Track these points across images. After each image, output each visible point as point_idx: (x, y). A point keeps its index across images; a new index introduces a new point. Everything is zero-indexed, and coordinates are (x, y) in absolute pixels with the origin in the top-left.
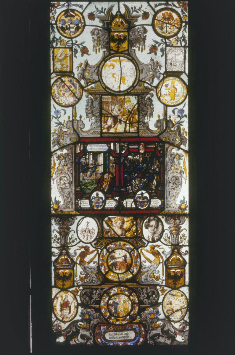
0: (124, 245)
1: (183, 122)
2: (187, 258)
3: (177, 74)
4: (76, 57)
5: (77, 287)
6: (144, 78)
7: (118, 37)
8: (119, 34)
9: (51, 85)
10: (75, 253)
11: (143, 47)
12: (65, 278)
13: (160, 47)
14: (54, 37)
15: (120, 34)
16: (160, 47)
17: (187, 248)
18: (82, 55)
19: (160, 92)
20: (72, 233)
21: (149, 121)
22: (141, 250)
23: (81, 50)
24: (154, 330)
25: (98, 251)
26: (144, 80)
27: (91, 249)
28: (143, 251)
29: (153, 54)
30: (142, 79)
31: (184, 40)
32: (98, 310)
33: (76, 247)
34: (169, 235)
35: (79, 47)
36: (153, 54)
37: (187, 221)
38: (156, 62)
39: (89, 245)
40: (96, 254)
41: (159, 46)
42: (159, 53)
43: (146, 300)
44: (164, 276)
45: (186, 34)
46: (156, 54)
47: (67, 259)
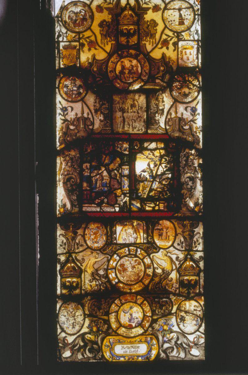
8: (129, 27)
18: (89, 50)
23: (88, 45)
36: (165, 48)
41: (171, 40)
42: (171, 47)
44: (177, 284)
46: (168, 48)
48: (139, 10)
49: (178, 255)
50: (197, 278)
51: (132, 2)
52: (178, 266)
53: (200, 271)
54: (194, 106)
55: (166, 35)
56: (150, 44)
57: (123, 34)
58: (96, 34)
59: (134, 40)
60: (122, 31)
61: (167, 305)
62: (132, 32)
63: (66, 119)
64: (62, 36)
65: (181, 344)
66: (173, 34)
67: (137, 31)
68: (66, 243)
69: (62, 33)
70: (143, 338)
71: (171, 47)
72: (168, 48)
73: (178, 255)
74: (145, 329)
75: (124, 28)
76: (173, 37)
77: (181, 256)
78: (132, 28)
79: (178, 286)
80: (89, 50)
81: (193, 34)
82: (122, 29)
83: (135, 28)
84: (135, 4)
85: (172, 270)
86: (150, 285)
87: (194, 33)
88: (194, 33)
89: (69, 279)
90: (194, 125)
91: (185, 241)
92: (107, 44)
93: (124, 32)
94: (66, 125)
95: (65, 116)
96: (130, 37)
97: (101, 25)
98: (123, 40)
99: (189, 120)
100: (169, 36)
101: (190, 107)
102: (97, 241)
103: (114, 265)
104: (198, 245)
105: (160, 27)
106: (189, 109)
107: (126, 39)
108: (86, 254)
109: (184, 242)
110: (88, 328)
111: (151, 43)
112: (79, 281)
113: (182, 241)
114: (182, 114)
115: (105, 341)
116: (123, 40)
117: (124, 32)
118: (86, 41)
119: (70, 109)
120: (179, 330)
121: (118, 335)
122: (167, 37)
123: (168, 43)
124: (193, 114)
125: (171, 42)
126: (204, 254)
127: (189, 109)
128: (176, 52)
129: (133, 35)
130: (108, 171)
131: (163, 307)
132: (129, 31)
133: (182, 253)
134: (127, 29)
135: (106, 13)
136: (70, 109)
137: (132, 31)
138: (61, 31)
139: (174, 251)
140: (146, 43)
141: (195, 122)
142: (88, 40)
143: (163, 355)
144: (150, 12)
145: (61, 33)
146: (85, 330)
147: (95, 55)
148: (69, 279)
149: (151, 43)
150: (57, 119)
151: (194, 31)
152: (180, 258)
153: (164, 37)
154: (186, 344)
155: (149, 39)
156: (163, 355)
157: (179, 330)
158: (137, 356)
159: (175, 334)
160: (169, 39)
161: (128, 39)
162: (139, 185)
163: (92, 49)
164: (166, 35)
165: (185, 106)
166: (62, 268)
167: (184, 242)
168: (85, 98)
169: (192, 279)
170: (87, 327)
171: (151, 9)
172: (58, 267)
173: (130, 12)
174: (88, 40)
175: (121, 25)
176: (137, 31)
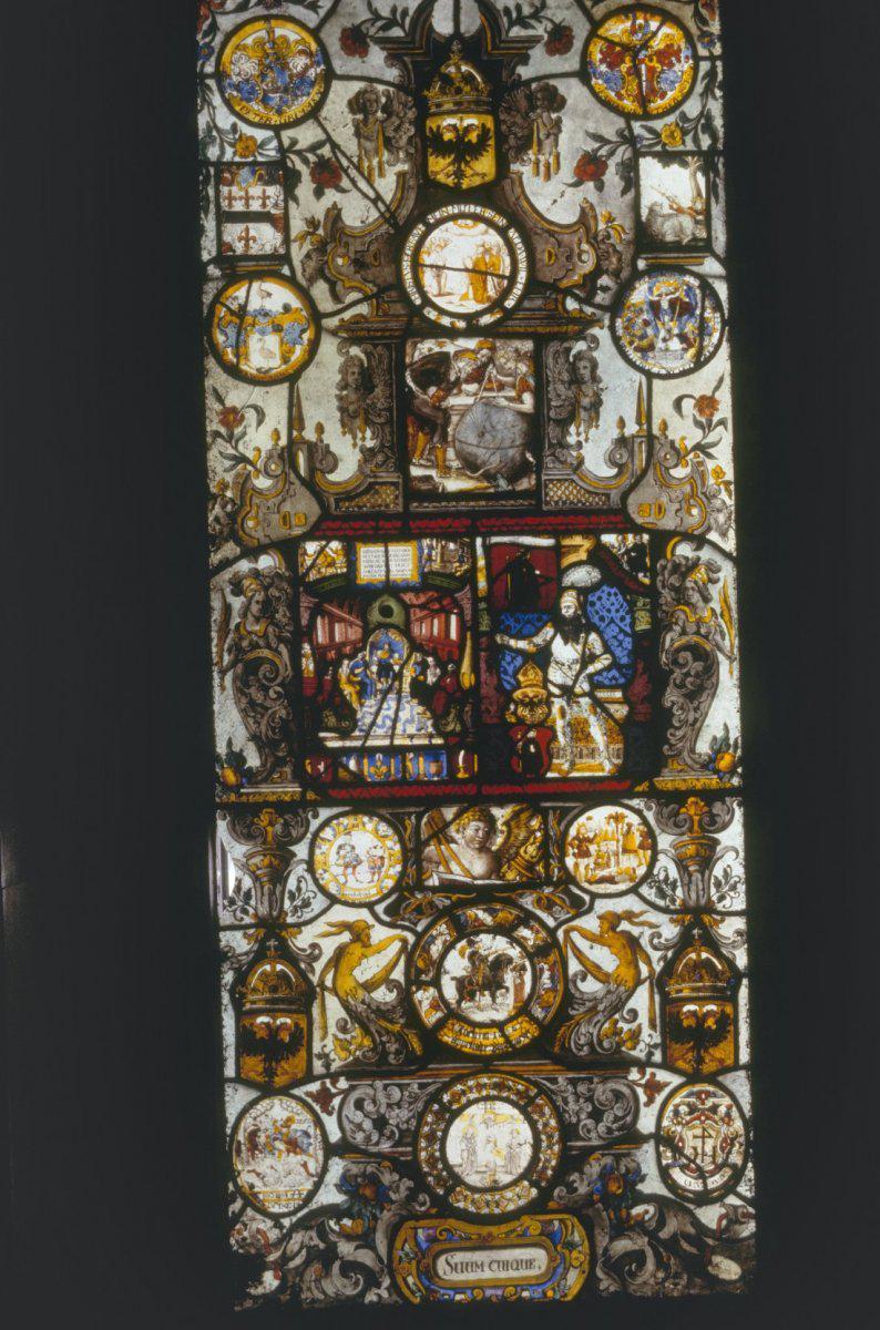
2: (741, 959)
4: (296, 200)
13: (617, 158)
14: (212, 126)
16: (617, 158)
18: (319, 193)
28: (575, 936)
31: (709, 128)
41: (612, 153)
45: (716, 108)
46: (600, 187)
48: (499, 49)
49: (658, 927)
51: (471, 22)
52: (658, 968)
53: (737, 976)
54: (709, 394)
56: (538, 174)
57: (443, 148)
59: (485, 165)
60: (438, 135)
64: (218, 141)
65: (674, 1238)
67: (491, 134)
68: (253, 893)
69: (218, 130)
70: (533, 1225)
71: (612, 177)
72: (600, 187)
73: (658, 927)
74: (224, 309)
75: (445, 124)
77: (670, 931)
78: (472, 125)
80: (319, 193)
81: (696, 128)
82: (439, 127)
84: (482, 26)
87: (699, 127)
88: (699, 127)
90: (710, 465)
91: (682, 881)
92: (381, 174)
94: (238, 476)
95: (237, 441)
96: (468, 159)
97: (358, 104)
98: (440, 167)
99: (690, 444)
101: (691, 397)
102: (326, 648)
104: (732, 894)
106: (688, 405)
107: (453, 163)
109: (679, 884)
110: (339, 1187)
111: (542, 169)
112: (303, 1025)
113: (671, 879)
114: (664, 426)
115: (402, 1235)
116: (440, 167)
118: (306, 161)
119: (251, 416)
120: (664, 1192)
122: (597, 145)
124: (704, 420)
125: (612, 164)
126: (748, 923)
127: (688, 405)
128: (630, 195)
129: (476, 150)
130: (732, 1028)
133: (672, 921)
134: (454, 127)
135: (377, 56)
136: (251, 416)
137: (473, 137)
138: (215, 124)
139: (646, 912)
140: (523, 169)
141: (711, 451)
142: (312, 158)
143: (606, 1284)
144: (537, 53)
145: (214, 133)
146: (330, 1196)
147: (340, 210)
149: (542, 169)
151: (699, 121)
152: (666, 940)
156: (606, 1284)
157: (664, 1192)
158: (516, 1286)
159: (651, 1209)
160: (603, 152)
161: (459, 168)
166: (242, 977)
167: (679, 884)
168: (316, 125)
169: (708, 1012)
170: (336, 1185)
172: (228, 977)
173: (464, 68)
174: (312, 158)
175: (435, 114)
176: (491, 134)
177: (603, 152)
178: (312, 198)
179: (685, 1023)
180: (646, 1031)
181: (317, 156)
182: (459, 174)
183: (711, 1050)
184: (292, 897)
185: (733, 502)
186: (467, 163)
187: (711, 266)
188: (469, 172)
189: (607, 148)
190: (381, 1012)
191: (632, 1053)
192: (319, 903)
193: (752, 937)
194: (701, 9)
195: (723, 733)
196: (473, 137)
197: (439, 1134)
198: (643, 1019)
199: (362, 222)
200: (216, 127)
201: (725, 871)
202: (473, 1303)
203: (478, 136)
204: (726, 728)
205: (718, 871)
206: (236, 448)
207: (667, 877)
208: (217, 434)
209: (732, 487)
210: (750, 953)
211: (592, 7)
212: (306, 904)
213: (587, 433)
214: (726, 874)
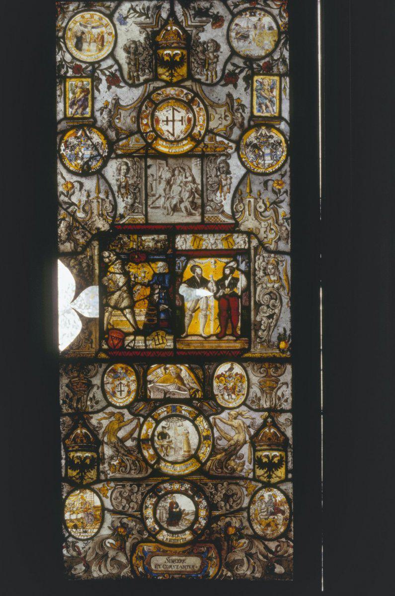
0: (197, 369)
1: (282, 201)
2: (289, 432)
3: (269, 123)
4: (99, 90)
5: (105, 483)
6: (216, 128)
7: (170, 57)
8: (173, 52)
9: (289, 158)
10: (99, 423)
11: (214, 73)
12: (83, 466)
13: (243, 74)
14: (63, 60)
15: (174, 53)
16: (243, 74)
17: (289, 416)
18: (109, 88)
19: (163, 84)
20: (95, 389)
21: (223, 200)
22: (214, 419)
23: (107, 80)
24: (240, 365)
25: (139, 419)
26: (215, 131)
27: (128, 416)
28: (218, 421)
29: (231, 86)
30: (214, 128)
31: (284, 62)
32: (142, 520)
33: (101, 415)
34: (259, 394)
35: (104, 74)
36: (231, 86)
37: (289, 368)
38: (221, 26)
39: (125, 411)
40: (137, 425)
41: (241, 72)
42: (241, 83)
43: (223, 504)
44: (251, 464)
45: (286, 54)
46: (235, 86)
47: (86, 435)
50: (283, 454)
55: (234, 65)
57: (164, 64)
58: (224, 424)
61: (125, 121)
62: (276, 462)
63: (72, 202)
66: (245, 63)
71: (241, 83)
75: (165, 52)
76: (244, 68)
79: (251, 467)
83: (182, 53)
85: (245, 442)
86: (209, 463)
89: (79, 454)
93: (165, 60)
95: (70, 197)
100: (238, 67)
103: (150, 432)
105: (225, 50)
108: (69, 324)
117: (165, 60)
121: (157, 541)
123: (237, 79)
131: (189, 365)
132: (271, 460)
137: (276, 460)
138: (64, 58)
148: (79, 454)
150: (98, 311)
153: (230, 67)
154: (263, 555)
155: (205, 72)
160: (237, 71)
162: (178, 272)
163: (113, 87)
164: (234, 65)
165: (262, 179)
171: (210, 23)
177: (237, 71)
178: (106, 90)
179: (264, 461)
180: (247, 463)
181: (109, 72)
182: (172, 75)
183: (275, 472)
184: (91, 399)
185: (290, 228)
186: (175, 70)
187: (283, 126)
188: (176, 74)
189: (239, 69)
190: (129, 451)
191: (241, 473)
192: (104, 403)
193: (295, 423)
194: (282, 12)
195: (283, 332)
196: (276, 460)
197: (90, 449)
198: (246, 458)
199: (135, 123)
200: (64, 60)
201: (283, 393)
202: (181, 578)
203: (278, 460)
204: (285, 329)
205: (279, 393)
206: (70, 199)
207: (256, 396)
208: (62, 193)
209: (290, 221)
210: (293, 429)
211: (234, 8)
212: (97, 403)
213: (225, 196)
214: (283, 395)
